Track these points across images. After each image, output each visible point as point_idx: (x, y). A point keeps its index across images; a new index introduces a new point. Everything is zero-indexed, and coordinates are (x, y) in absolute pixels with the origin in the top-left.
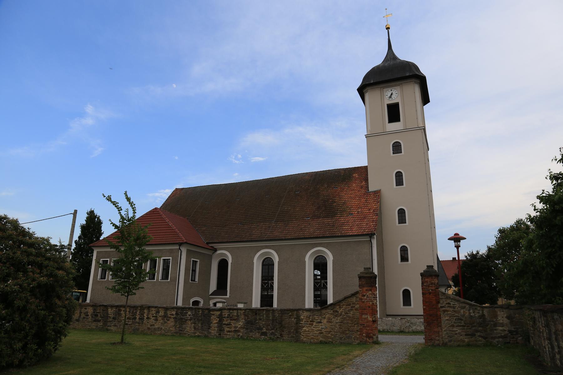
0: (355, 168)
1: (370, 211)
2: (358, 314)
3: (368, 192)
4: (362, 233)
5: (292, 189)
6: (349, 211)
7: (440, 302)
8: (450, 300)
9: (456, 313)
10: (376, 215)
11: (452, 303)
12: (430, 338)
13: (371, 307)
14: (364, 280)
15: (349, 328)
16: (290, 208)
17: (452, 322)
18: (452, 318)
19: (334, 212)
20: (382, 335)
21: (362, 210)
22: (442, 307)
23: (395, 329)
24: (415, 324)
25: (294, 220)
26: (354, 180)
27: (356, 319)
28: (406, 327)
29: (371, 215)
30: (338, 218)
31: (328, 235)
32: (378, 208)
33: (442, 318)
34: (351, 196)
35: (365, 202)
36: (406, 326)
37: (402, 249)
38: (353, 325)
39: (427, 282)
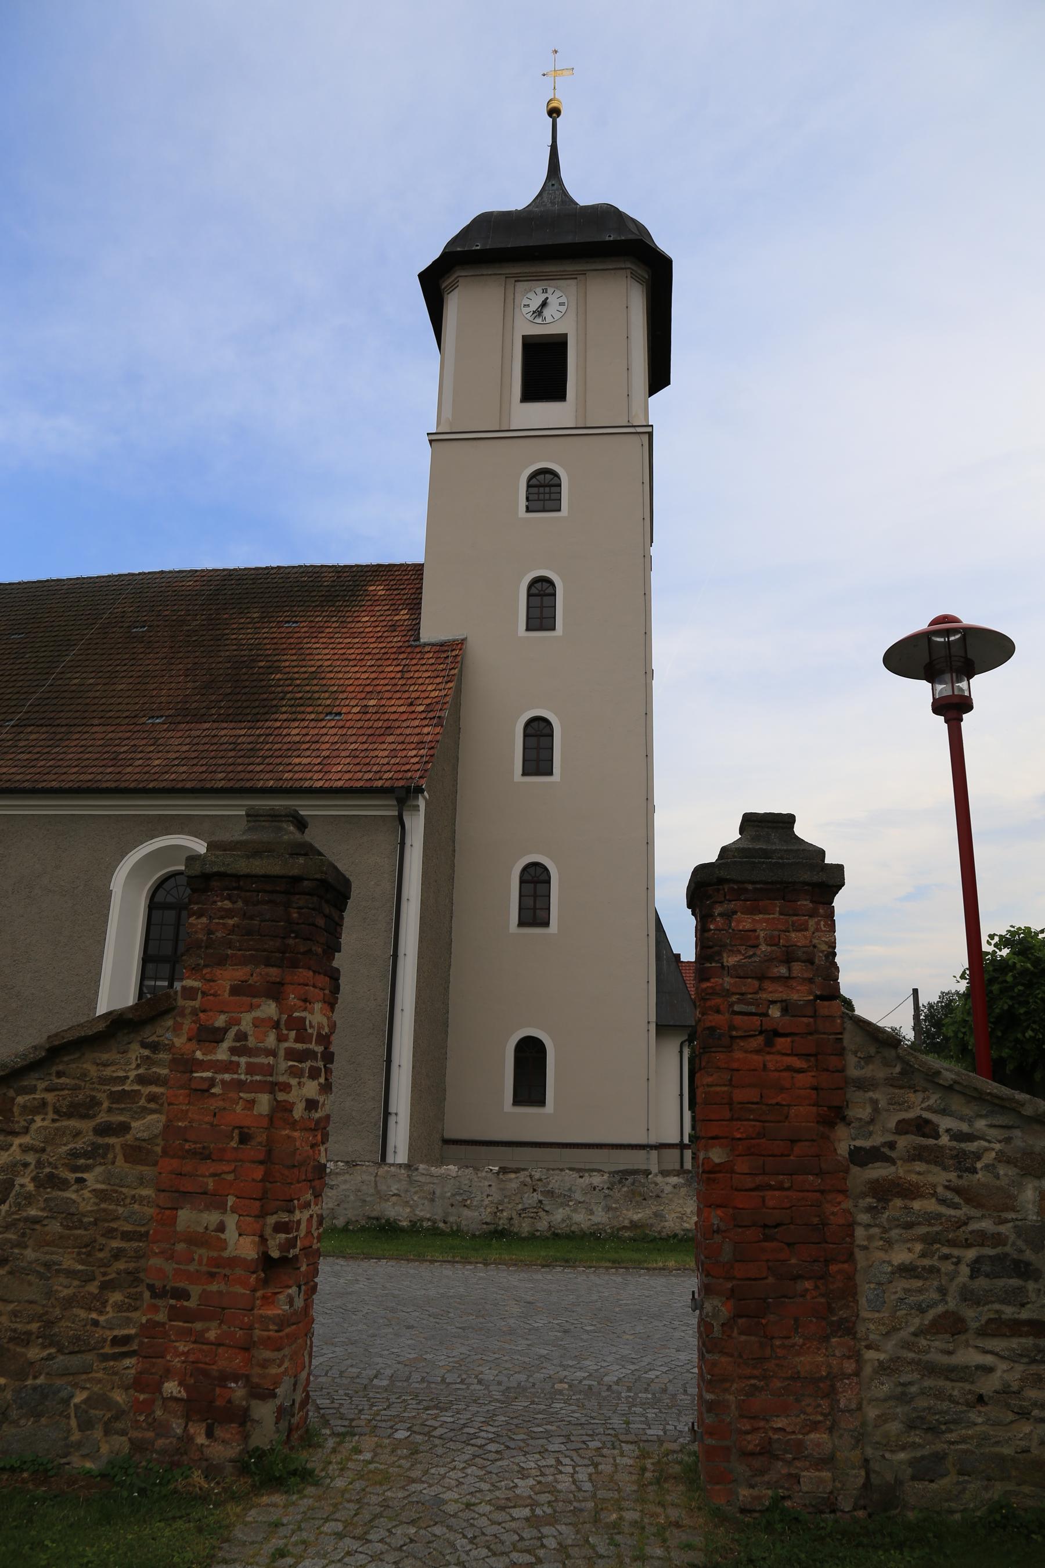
0: (379, 566)
1: (412, 708)
2: (145, 1192)
3: (417, 643)
4: (368, 785)
5: (123, 617)
6: (328, 702)
7: (852, 1113)
8: (934, 1099)
9: (979, 1206)
10: (435, 721)
11: (945, 1123)
12: (753, 1442)
13: (262, 1137)
14: (227, 904)
15: (57, 1312)
16: (91, 681)
17: (943, 1291)
18: (946, 1250)
19: (266, 703)
20: (398, 1258)
21: (383, 702)
22: (861, 1157)
23: (472, 1218)
24: (564, 1198)
25: (96, 722)
26: (369, 603)
27: (126, 1236)
28: (524, 1209)
29: (416, 723)
30: (278, 724)
31: (220, 784)
32: (447, 699)
33: (859, 1255)
34: (349, 652)
35: (399, 675)
36: (520, 1206)
37: (527, 877)
38: (93, 1288)
39: (748, 939)
